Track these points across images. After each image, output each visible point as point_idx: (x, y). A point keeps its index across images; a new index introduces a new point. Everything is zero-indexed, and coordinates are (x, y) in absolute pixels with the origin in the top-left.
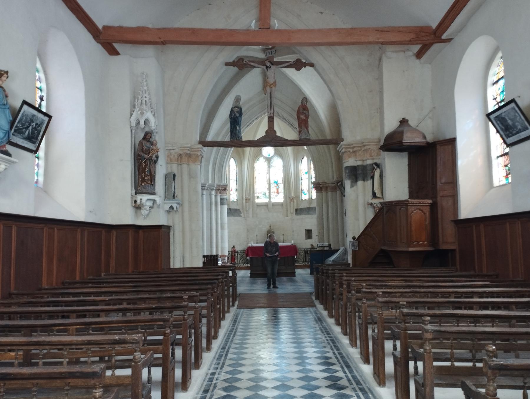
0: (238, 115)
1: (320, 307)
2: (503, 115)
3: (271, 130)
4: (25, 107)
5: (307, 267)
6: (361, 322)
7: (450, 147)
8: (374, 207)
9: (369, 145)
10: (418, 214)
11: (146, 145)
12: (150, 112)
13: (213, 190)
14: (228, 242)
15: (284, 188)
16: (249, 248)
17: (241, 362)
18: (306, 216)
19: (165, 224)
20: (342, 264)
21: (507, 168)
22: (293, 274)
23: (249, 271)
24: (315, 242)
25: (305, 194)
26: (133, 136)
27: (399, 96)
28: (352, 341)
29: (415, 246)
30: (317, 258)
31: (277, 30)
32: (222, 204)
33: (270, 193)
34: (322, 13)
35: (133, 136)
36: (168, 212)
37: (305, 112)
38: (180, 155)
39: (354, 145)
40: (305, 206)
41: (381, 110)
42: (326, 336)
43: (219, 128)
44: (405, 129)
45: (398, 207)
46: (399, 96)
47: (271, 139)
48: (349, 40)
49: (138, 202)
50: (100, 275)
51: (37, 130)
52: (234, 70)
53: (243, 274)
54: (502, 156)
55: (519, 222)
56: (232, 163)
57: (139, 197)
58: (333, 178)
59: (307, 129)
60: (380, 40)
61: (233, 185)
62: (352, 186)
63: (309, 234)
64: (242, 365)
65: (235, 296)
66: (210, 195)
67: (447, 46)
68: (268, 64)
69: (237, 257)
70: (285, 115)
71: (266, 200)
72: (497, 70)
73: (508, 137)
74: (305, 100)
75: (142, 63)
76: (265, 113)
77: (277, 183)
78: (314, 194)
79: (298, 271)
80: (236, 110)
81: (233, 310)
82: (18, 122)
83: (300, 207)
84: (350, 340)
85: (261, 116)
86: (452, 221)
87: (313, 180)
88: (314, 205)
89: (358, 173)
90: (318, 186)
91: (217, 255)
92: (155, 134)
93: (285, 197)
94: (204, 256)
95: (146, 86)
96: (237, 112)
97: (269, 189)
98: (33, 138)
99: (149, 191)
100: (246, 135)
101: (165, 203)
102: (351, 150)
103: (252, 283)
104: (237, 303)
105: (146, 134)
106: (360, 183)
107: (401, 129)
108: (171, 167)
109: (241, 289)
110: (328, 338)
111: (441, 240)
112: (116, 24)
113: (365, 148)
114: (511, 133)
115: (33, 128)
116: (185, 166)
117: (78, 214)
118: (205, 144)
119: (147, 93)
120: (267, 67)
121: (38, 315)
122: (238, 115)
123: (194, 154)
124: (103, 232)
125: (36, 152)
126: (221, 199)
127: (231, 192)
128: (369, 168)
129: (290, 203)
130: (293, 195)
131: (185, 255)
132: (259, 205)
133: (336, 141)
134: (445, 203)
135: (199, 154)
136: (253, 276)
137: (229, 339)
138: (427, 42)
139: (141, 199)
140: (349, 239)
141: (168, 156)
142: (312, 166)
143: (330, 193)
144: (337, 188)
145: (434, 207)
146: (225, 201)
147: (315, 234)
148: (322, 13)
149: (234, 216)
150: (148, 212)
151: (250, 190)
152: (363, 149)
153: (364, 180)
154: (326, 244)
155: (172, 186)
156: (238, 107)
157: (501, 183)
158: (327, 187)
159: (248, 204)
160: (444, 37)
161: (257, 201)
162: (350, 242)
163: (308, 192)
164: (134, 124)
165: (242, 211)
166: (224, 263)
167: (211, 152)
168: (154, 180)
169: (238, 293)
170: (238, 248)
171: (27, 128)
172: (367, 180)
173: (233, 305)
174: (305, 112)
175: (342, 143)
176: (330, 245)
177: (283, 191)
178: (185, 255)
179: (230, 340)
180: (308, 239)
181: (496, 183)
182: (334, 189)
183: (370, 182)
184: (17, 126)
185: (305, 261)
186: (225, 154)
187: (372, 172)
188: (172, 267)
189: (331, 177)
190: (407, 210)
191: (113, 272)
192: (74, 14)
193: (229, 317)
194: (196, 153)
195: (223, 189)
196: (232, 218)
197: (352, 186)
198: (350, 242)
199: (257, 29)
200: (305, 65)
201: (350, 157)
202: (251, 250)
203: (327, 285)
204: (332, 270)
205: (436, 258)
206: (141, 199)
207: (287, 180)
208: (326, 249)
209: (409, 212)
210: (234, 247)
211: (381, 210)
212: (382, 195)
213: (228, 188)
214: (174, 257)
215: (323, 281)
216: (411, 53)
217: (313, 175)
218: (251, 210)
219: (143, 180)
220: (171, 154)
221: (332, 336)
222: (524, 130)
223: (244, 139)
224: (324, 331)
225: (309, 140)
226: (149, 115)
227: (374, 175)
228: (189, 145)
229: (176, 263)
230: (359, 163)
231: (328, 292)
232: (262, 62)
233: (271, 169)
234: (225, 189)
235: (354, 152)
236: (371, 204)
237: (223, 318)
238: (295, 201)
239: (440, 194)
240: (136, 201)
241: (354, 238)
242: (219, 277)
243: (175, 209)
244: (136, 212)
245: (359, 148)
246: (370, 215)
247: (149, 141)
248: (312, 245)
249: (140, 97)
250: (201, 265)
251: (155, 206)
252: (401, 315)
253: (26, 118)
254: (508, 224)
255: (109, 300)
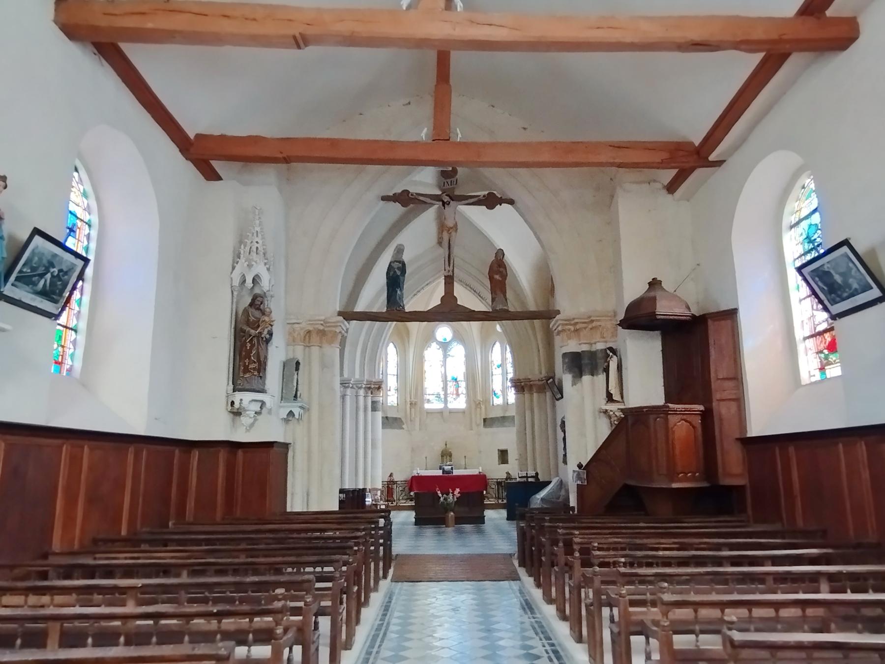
0: (399, 273)
1: (528, 581)
2: (825, 267)
3: (449, 296)
4: (38, 240)
5: (502, 506)
6: (616, 630)
7: (729, 322)
8: (610, 417)
9: (598, 321)
10: (682, 425)
11: (254, 314)
12: (263, 264)
13: (360, 388)
14: (383, 468)
15: (467, 388)
16: (413, 477)
17: (402, 653)
18: (500, 429)
19: (282, 440)
20: (558, 508)
21: (822, 355)
22: (481, 520)
23: (413, 514)
24: (514, 469)
25: (498, 397)
26: (235, 300)
27: (648, 245)
28: (595, 660)
29: (680, 481)
30: (517, 495)
31: (460, 143)
32: (374, 409)
33: (446, 395)
34: (525, 129)
35: (235, 300)
36: (286, 421)
37: (501, 269)
38: (309, 332)
39: (576, 321)
40: (499, 414)
41: (616, 269)
42: (544, 641)
43: (372, 295)
44: (658, 294)
45: (652, 417)
46: (648, 245)
47: (449, 311)
48: (571, 159)
49: (237, 405)
50: (167, 527)
51: (60, 280)
52: (397, 209)
53: (403, 519)
54: (812, 336)
55: (863, 443)
56: (391, 351)
57: (238, 396)
58: (541, 373)
59: (505, 296)
60: (617, 161)
61: (392, 382)
62: (574, 384)
63: (503, 456)
64: (411, 624)
65: (388, 558)
66: (357, 396)
67: (718, 174)
68: (446, 199)
69: (397, 490)
70: (470, 281)
71: (439, 406)
72: (804, 202)
73: (834, 302)
74: (500, 254)
75: (256, 194)
76: (439, 277)
77: (456, 380)
78: (512, 396)
79: (489, 514)
80: (396, 265)
81: (384, 584)
82: (24, 265)
83: (491, 416)
84: (590, 656)
85: (433, 281)
86: (737, 439)
87: (510, 376)
88: (512, 412)
89: (580, 364)
90: (520, 385)
91: (364, 490)
92: (269, 298)
93: (468, 402)
94: (342, 491)
95: (260, 225)
96: (398, 268)
97: (445, 388)
98: (54, 293)
99: (255, 387)
100: (411, 305)
101: (281, 407)
102: (572, 328)
103: (418, 535)
104: (391, 572)
105: (255, 298)
106: (586, 378)
107: (652, 294)
108: (294, 351)
109: (399, 546)
110: (548, 648)
111: (720, 470)
112: (217, 133)
113: (594, 324)
114: (839, 296)
115: (53, 276)
116: (315, 350)
117: (137, 424)
118: (349, 315)
119: (259, 235)
120: (444, 204)
121: (109, 572)
122: (399, 273)
123: (330, 331)
124: (177, 451)
125: (57, 317)
126: (373, 403)
127: (389, 393)
128: (600, 355)
129: (476, 409)
130: (479, 398)
131: (310, 492)
132: (430, 413)
133: (546, 315)
134: (724, 410)
135: (338, 331)
136: (419, 522)
137: (373, 647)
138: (687, 166)
139: (241, 400)
140: (572, 466)
141: (290, 334)
142: (509, 355)
143: (535, 395)
144: (547, 387)
145: (707, 416)
146: (380, 406)
147: (512, 456)
148: (525, 129)
149: (392, 428)
150: (252, 420)
151: (417, 389)
152: (590, 326)
153: (593, 375)
154: (531, 473)
155: (293, 380)
156: (399, 262)
157: (813, 379)
158: (531, 385)
159: (413, 410)
160: (712, 158)
161: (427, 406)
162: (574, 471)
163: (503, 394)
164: (236, 282)
165: (403, 420)
166: (375, 500)
167: (361, 330)
168: (265, 369)
169: (394, 553)
170: (396, 478)
171: (42, 276)
172: (597, 374)
173: (385, 577)
174: (501, 269)
175: (558, 317)
176: (537, 474)
177: (465, 392)
178: (310, 492)
179: (375, 650)
180: (503, 463)
181: (805, 378)
182: (541, 389)
183: (602, 377)
184: (20, 272)
185: (499, 498)
186: (380, 334)
187: (606, 361)
188: (289, 510)
189: (537, 372)
190: (667, 420)
191: (192, 520)
192: (149, 111)
193: (376, 599)
194: (334, 329)
195: (376, 387)
196: (389, 431)
197: (574, 384)
198: (574, 471)
199: (430, 141)
200: (501, 201)
201: (569, 338)
202: (417, 482)
203: (541, 545)
204: (550, 521)
205: (713, 500)
206: (241, 400)
207: (470, 377)
208: (530, 480)
209: (671, 424)
210: (391, 475)
211: (621, 421)
212: (622, 397)
213: (383, 386)
214: (292, 494)
215: (532, 538)
216: (659, 186)
217: (510, 370)
218: (417, 420)
219: (246, 370)
220: (294, 331)
221: (553, 641)
222: (864, 291)
223: (408, 309)
224: (539, 630)
225: (507, 311)
226: (260, 269)
227: (608, 366)
228: (323, 318)
229: (296, 504)
230: (585, 348)
231: (543, 559)
232: (436, 198)
233: (448, 360)
234: (379, 388)
235: (576, 330)
236: (606, 412)
237: (366, 603)
238: (483, 407)
239: (717, 396)
240: (233, 403)
241: (580, 466)
242: (359, 534)
243: (297, 416)
244: (233, 421)
245: (584, 325)
246: (604, 431)
247: (259, 309)
248: (508, 473)
249: (249, 242)
250: (335, 507)
251: (264, 411)
252: (728, 645)
253: (40, 259)
254: (841, 446)
255: (144, 586)
